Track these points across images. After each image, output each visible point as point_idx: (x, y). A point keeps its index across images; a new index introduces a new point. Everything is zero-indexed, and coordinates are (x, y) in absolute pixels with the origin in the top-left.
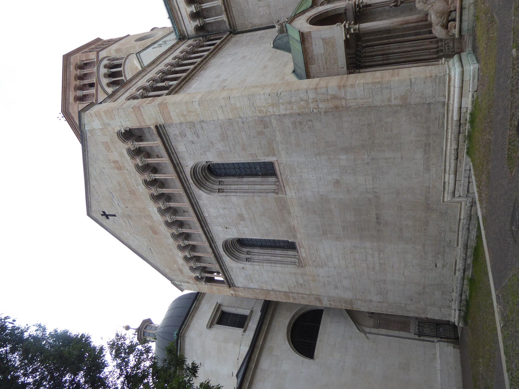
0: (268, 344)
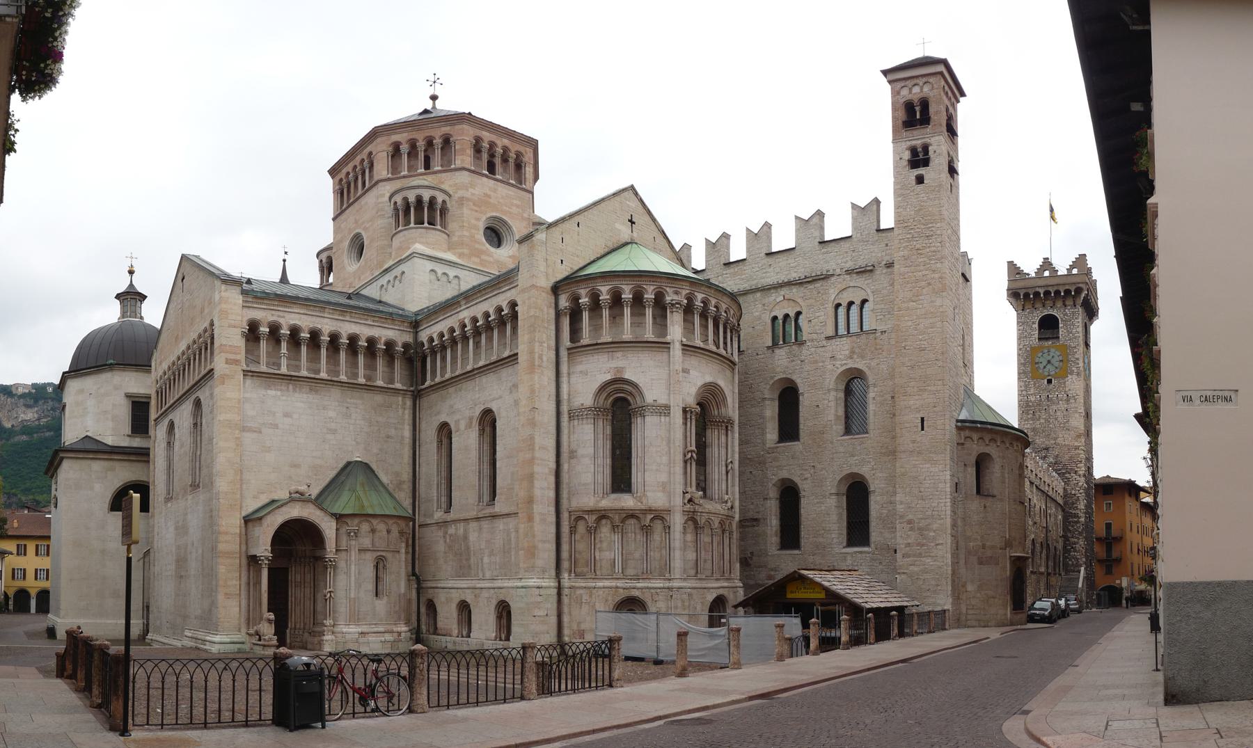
0: (117, 464)
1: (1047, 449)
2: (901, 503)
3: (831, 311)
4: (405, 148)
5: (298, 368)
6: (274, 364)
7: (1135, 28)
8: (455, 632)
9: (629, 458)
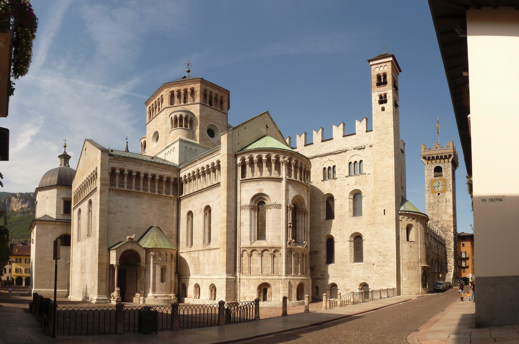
1: (438, 222)
2: (376, 244)
3: (347, 165)
4: (176, 93)
5: (131, 188)
6: (121, 186)
7: (461, 36)
8: (193, 297)
9: (265, 226)
